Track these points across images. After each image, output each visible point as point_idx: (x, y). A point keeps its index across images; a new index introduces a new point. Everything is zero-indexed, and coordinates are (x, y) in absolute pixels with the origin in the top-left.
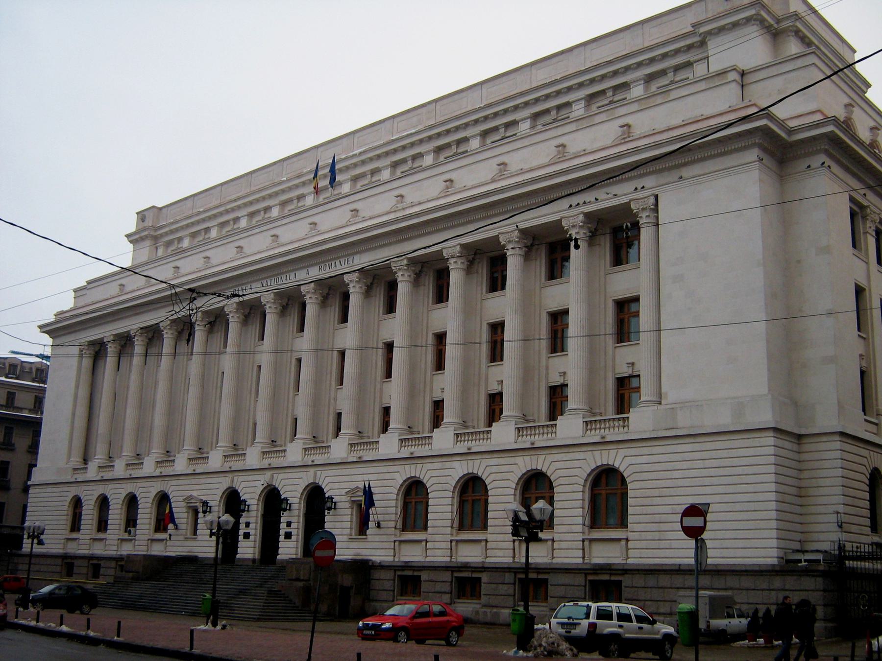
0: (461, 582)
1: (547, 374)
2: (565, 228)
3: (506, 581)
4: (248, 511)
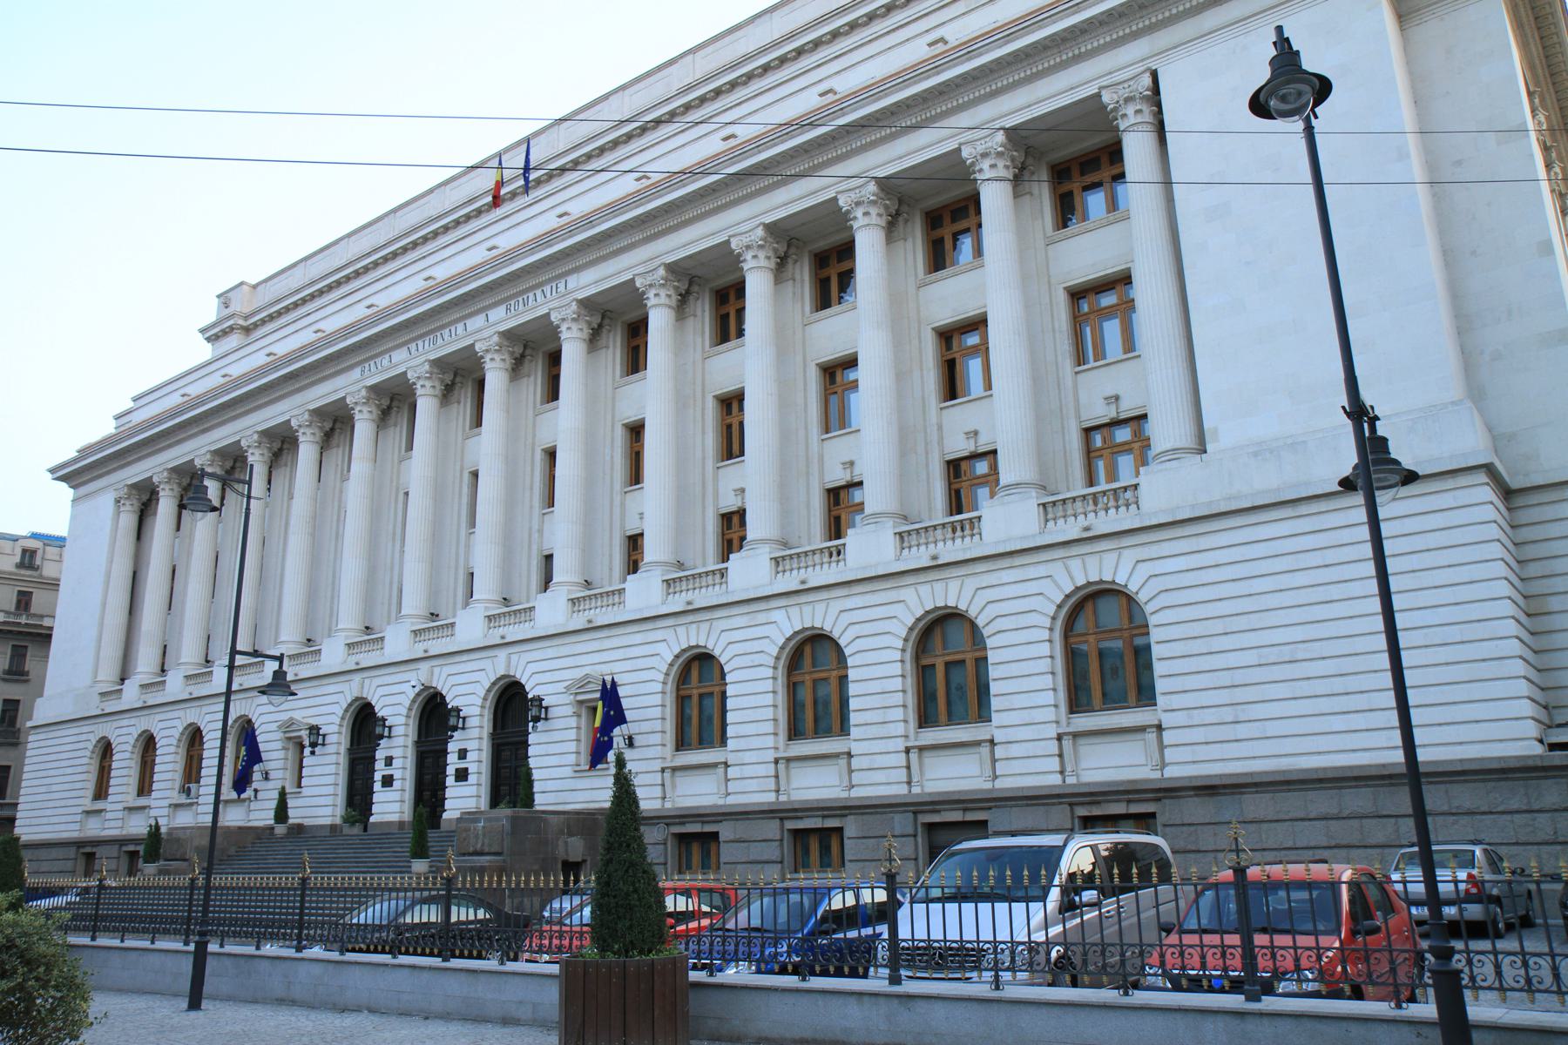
0: (683, 839)
1: (941, 439)
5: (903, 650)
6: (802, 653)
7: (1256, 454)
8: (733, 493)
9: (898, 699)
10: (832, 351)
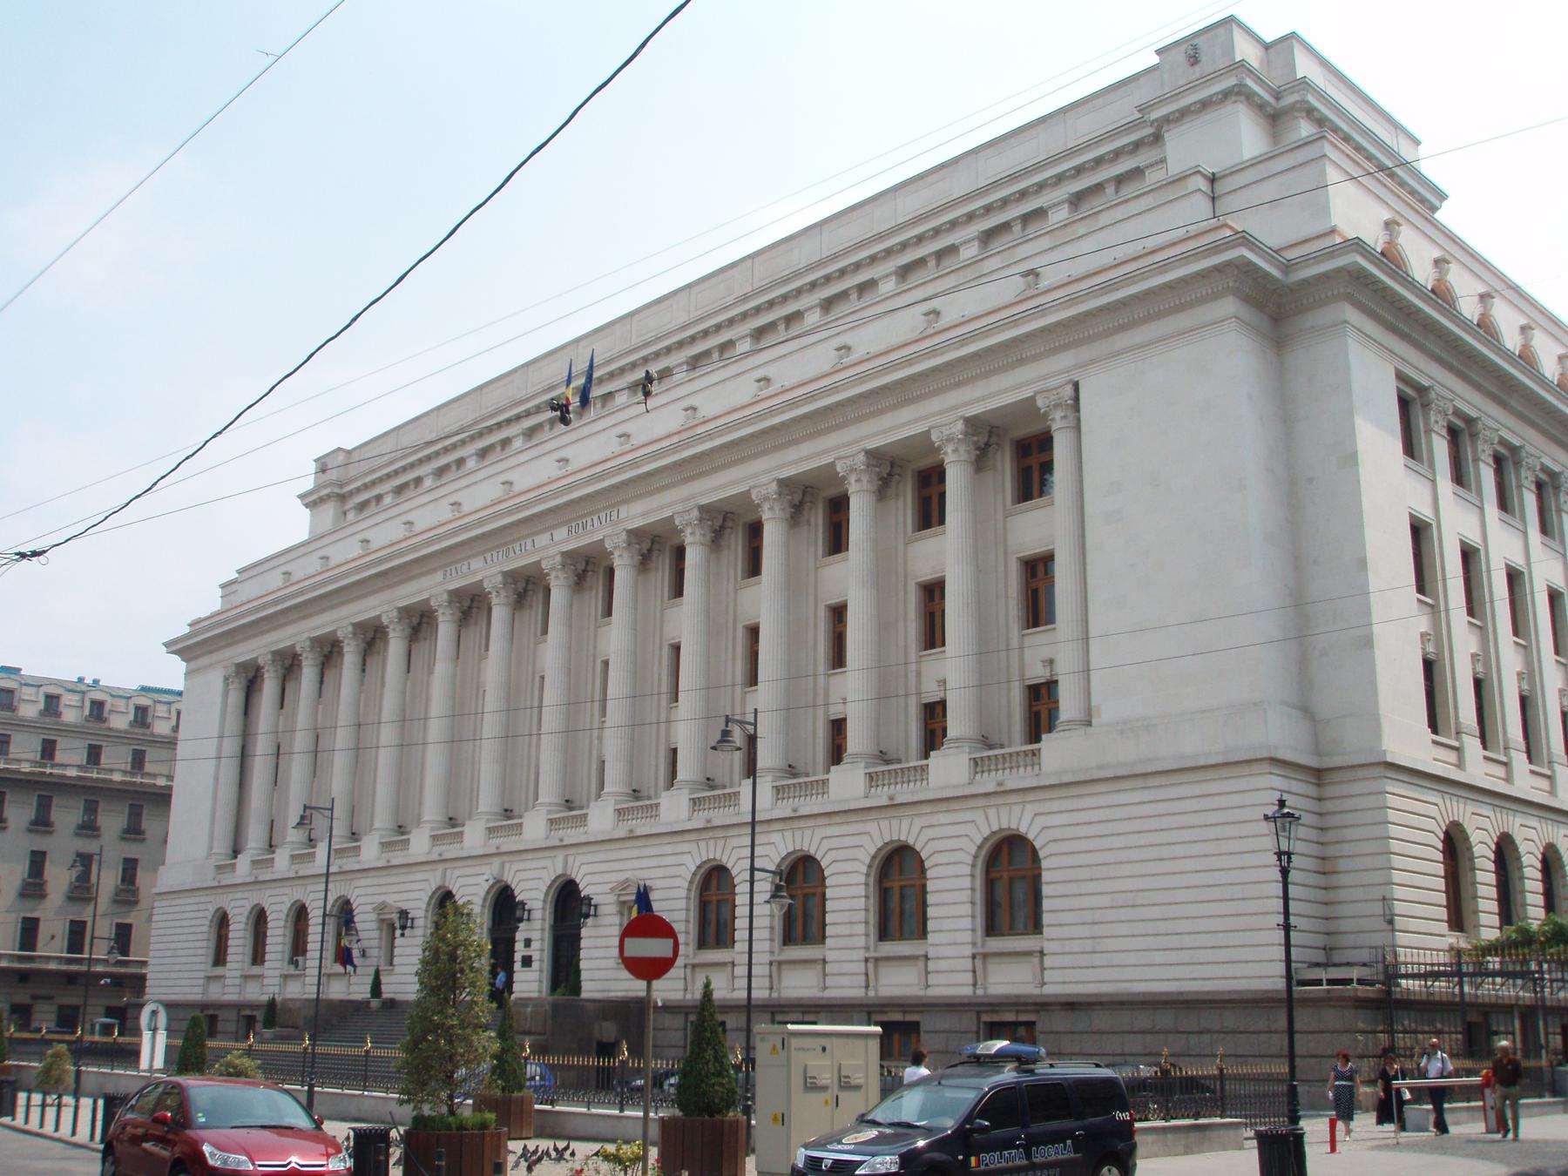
2: (1043, 410)
4: (529, 920)
7: (1122, 732)
8: (1041, 664)
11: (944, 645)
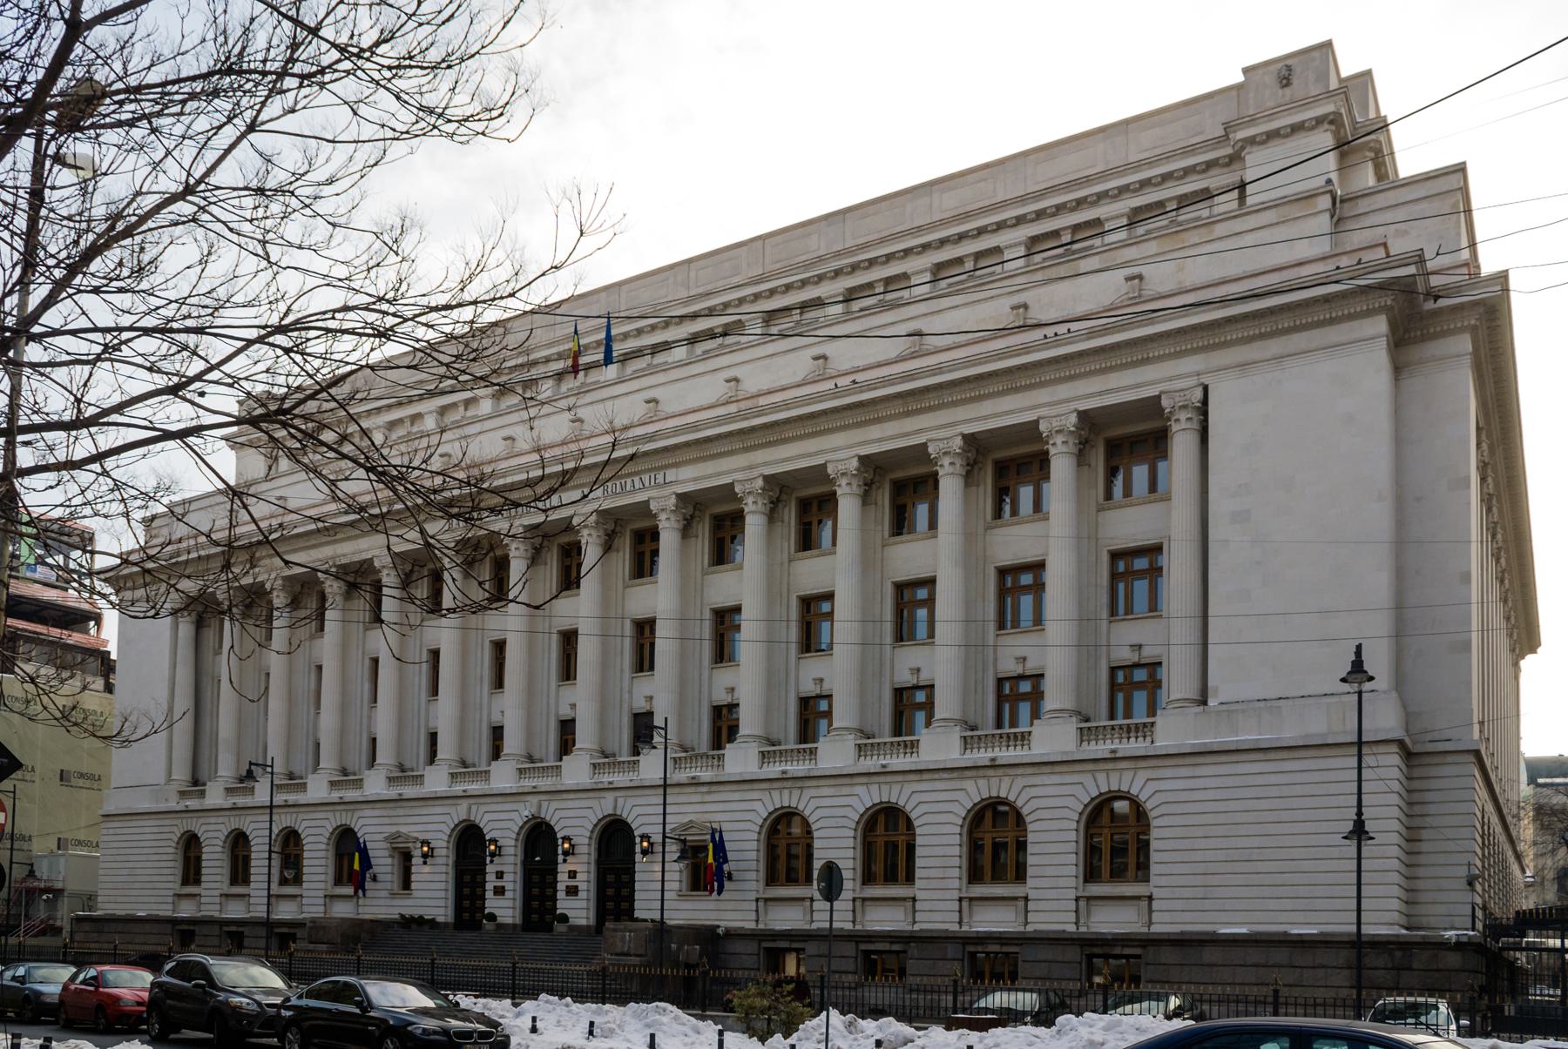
3: (949, 956)
5: (759, 833)
6: (983, 817)
9: (956, 862)
10: (811, 587)
11: (575, 679)
